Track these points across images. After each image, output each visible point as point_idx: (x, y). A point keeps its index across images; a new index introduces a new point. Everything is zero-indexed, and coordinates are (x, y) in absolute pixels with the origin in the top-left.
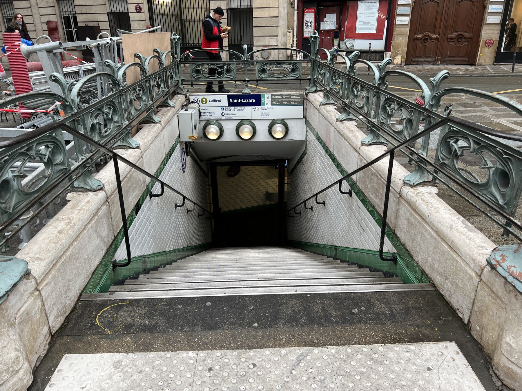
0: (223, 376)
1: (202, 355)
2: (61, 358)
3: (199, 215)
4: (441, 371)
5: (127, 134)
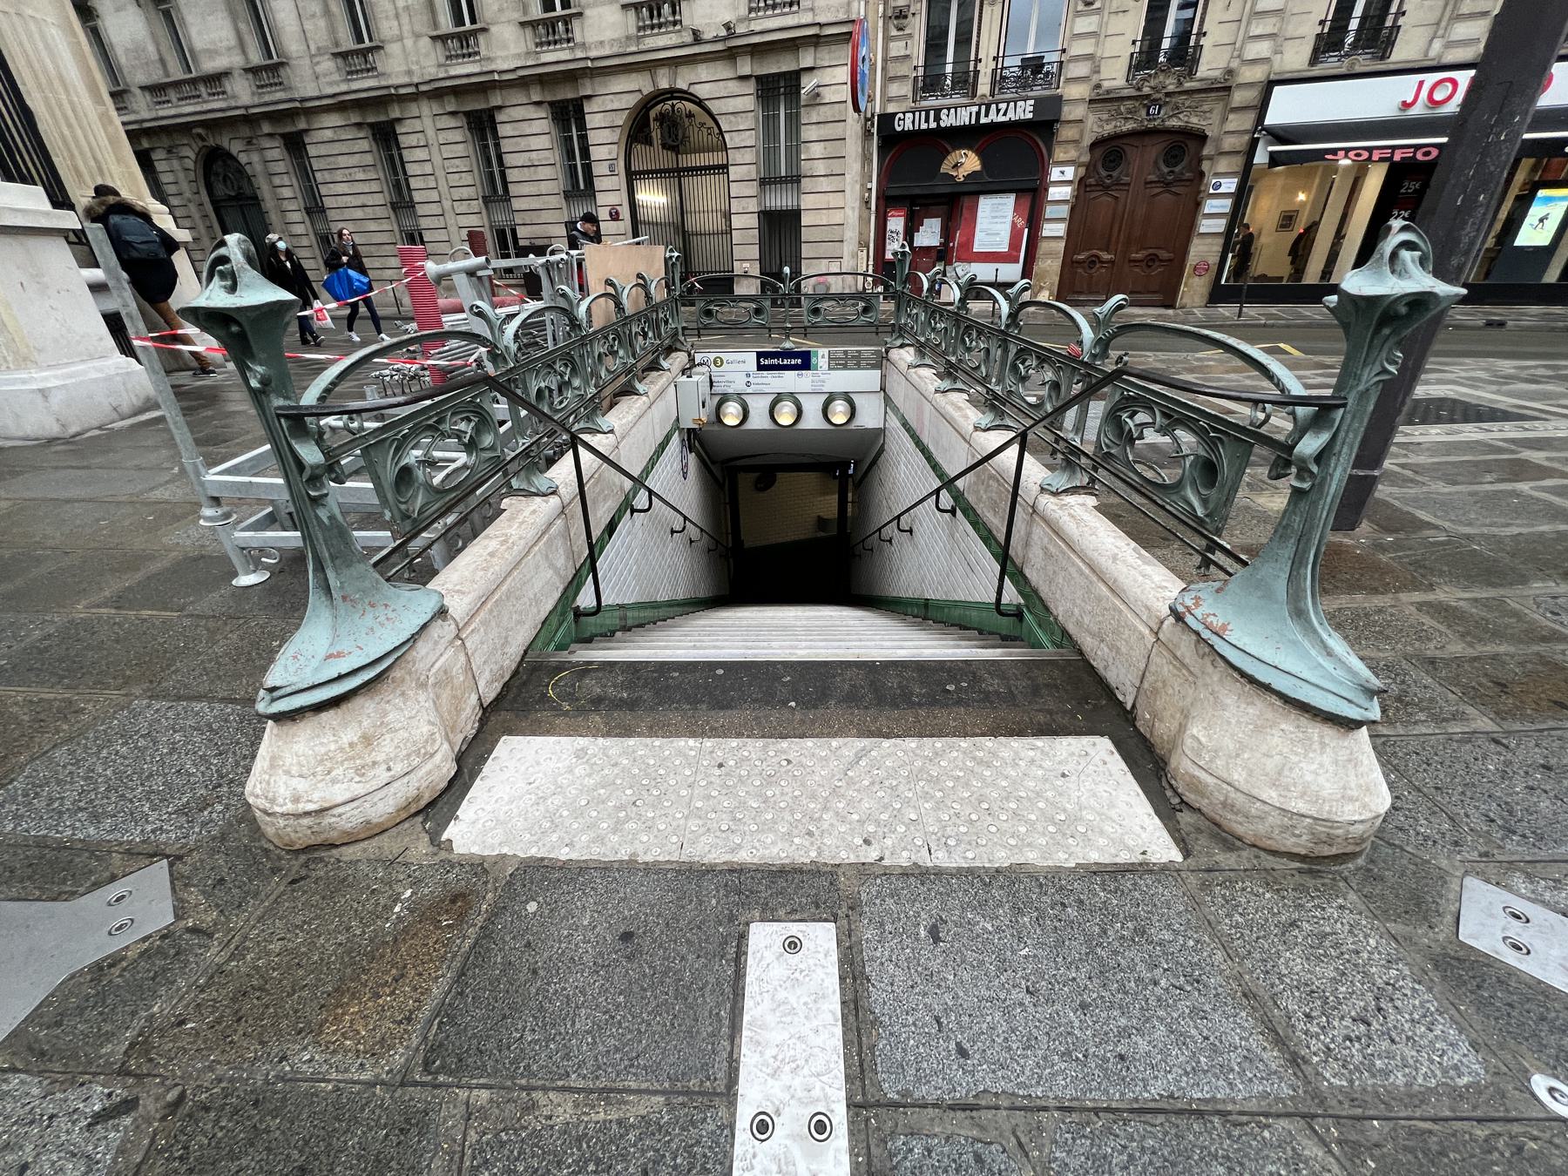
0: (740, 776)
1: (709, 744)
2: (497, 741)
3: (709, 550)
4: (1082, 778)
5: (594, 410)
